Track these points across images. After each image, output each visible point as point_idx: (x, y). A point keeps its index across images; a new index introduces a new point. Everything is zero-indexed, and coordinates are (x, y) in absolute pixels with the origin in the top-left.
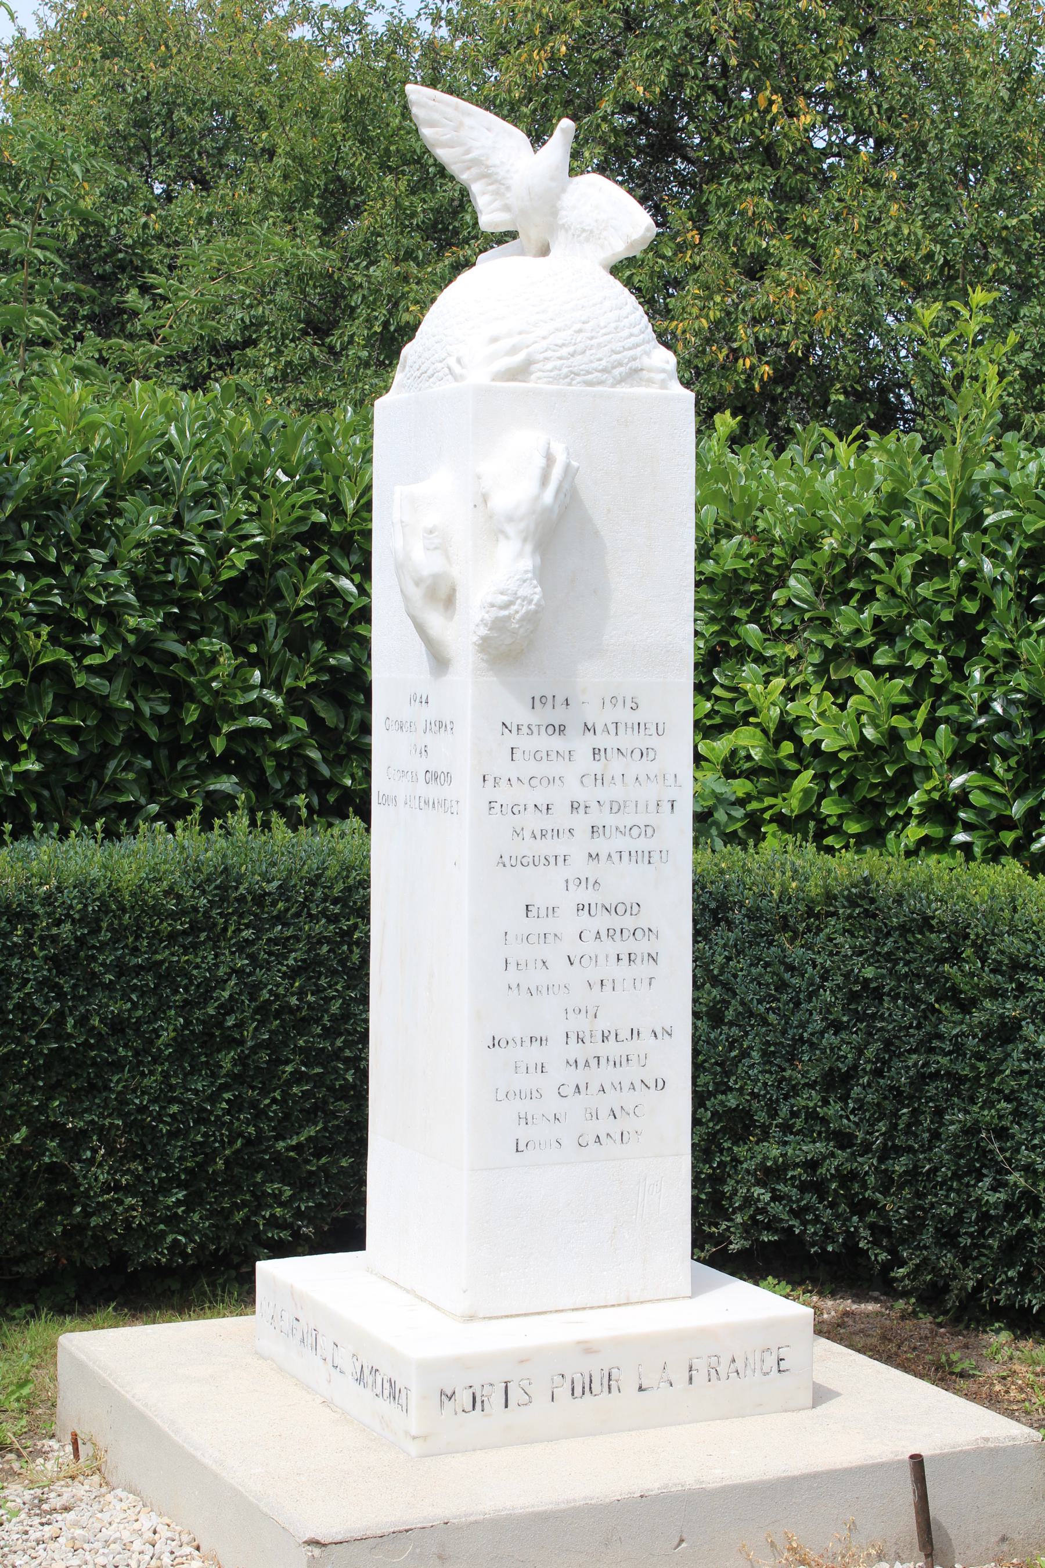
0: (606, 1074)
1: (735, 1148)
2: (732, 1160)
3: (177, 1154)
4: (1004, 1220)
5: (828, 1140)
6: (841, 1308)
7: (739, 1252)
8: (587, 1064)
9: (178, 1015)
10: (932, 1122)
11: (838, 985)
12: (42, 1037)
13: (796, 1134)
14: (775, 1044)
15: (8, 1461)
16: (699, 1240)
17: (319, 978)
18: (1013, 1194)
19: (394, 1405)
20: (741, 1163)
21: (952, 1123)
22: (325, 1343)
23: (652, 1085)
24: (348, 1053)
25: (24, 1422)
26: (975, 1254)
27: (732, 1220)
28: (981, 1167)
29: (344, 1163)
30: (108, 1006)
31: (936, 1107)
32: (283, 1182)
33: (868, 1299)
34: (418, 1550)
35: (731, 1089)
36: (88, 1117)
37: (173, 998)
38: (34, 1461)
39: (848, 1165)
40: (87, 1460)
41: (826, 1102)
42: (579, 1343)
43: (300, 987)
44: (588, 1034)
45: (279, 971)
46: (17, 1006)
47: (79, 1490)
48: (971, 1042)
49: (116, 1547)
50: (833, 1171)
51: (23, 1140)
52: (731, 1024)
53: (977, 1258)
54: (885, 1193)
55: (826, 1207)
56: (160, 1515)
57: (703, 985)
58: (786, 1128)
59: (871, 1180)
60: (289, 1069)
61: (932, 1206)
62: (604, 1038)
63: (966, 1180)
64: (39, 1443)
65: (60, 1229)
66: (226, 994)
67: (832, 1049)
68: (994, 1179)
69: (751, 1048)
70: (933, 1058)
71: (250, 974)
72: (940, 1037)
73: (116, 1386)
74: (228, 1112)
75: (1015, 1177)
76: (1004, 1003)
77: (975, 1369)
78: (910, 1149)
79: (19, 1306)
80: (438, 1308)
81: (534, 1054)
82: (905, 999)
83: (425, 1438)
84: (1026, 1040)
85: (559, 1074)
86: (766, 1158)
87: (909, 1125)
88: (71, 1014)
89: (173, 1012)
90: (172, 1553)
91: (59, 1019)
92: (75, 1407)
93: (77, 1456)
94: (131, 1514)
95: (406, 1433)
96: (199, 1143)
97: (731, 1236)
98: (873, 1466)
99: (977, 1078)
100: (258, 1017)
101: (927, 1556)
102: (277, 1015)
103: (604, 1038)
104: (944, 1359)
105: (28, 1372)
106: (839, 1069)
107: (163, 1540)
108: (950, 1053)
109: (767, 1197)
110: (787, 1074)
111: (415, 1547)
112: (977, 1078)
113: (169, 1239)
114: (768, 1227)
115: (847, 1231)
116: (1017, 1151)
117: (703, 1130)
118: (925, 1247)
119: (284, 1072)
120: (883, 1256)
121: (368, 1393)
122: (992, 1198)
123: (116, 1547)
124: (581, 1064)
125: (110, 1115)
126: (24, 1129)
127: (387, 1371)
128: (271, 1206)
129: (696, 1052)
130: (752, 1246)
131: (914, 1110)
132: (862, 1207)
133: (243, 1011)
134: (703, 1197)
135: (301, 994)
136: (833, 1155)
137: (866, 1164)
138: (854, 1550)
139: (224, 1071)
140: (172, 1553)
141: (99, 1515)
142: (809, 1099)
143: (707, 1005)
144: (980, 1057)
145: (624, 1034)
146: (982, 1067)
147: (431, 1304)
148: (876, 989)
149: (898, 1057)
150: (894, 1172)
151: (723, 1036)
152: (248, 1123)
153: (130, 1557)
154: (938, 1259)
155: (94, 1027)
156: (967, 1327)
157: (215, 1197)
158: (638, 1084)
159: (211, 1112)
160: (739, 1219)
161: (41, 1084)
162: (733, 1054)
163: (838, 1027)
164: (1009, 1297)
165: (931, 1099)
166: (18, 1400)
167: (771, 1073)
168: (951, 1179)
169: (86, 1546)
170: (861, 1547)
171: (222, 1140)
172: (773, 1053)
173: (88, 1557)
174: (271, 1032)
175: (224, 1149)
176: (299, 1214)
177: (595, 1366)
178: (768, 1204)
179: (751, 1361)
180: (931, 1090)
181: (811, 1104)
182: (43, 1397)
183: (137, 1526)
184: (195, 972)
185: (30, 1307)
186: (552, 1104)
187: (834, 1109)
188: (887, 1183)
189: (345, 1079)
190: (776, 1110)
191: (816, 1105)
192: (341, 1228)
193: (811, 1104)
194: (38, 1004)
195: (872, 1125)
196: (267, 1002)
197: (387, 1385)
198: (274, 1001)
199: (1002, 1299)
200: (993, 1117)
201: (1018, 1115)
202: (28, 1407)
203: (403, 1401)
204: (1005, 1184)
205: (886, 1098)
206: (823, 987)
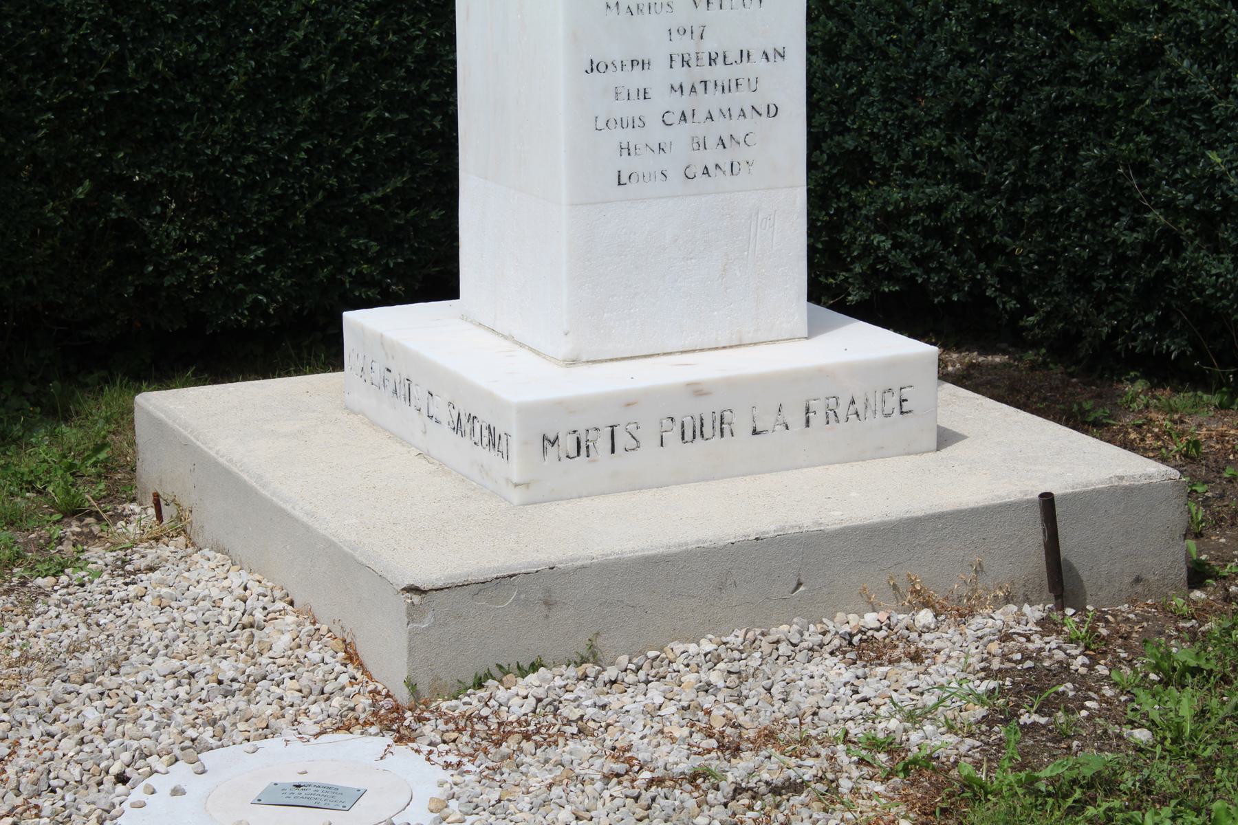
0: (713, 101)
1: (854, 194)
2: (850, 206)
3: (254, 209)
4: (1141, 262)
5: (953, 181)
6: (967, 360)
7: (858, 303)
8: (693, 89)
9: (248, 58)
10: (1065, 159)
11: (964, 14)
12: (101, 82)
13: (921, 175)
14: (896, 79)
15: (87, 525)
16: (816, 293)
17: (401, 16)
18: (1153, 234)
19: (493, 453)
20: (860, 209)
21: (1087, 159)
22: (418, 392)
23: (764, 111)
24: (434, 98)
25: (102, 486)
26: (1110, 299)
27: (849, 270)
28: (1118, 206)
29: (434, 216)
30: (172, 49)
31: (1070, 143)
32: (368, 237)
33: (994, 352)
34: (523, 596)
35: (848, 130)
36: (156, 170)
37: (242, 39)
38: (115, 524)
39: (974, 208)
40: (173, 523)
41: (950, 141)
42: (689, 385)
43: (380, 25)
44: (694, 57)
45: (357, 8)
46: (73, 49)
47: (164, 551)
48: (1109, 70)
49: (207, 604)
50: (958, 215)
51: (87, 195)
52: (848, 59)
53: (1111, 303)
54: (1014, 236)
55: (950, 254)
56: (251, 572)
57: (818, 17)
58: (908, 170)
59: (1000, 223)
60: (371, 115)
61: (1065, 249)
62: (712, 61)
63: (1102, 220)
64: (120, 508)
65: (131, 290)
66: (300, 34)
67: (958, 83)
68: (1132, 218)
69: (870, 84)
70: (1067, 89)
71: (325, 12)
72: (1075, 66)
73: (198, 443)
74: (307, 162)
75: (1156, 216)
76: (1146, 25)
77: (1109, 417)
78: (1041, 189)
79: (92, 373)
80: (538, 353)
81: (636, 79)
82: (1037, 26)
83: (527, 485)
84: (1169, 65)
85: (662, 100)
86: (886, 203)
87: (1040, 163)
88: (132, 57)
89: (243, 54)
90: (265, 609)
91: (119, 62)
92: (155, 467)
93: (159, 516)
94: (220, 572)
95: (508, 480)
96: (278, 196)
97: (842, 278)
98: (1000, 506)
99: (1115, 109)
100: (336, 59)
101: (1057, 597)
102: (357, 56)
103: (712, 61)
104: (1076, 407)
105: (105, 437)
106: (965, 105)
107: (254, 595)
108: (1086, 83)
109: (888, 245)
110: (909, 112)
111: (519, 593)
112: (1115, 109)
113: (249, 299)
114: (890, 277)
115: (974, 279)
116: (1158, 186)
117: (819, 174)
118: (1057, 293)
119: (366, 119)
120: (1012, 304)
121: (466, 442)
122: (1129, 238)
123: (207, 604)
124: (687, 89)
125: (180, 167)
126: (87, 183)
127: (485, 418)
128: (357, 263)
129: (810, 90)
130: (871, 297)
131: (1046, 147)
132: (988, 252)
133: (320, 53)
134: (820, 246)
135: (382, 34)
136: (958, 197)
137: (994, 207)
138: (980, 591)
139: (301, 118)
140: (265, 609)
141: (186, 574)
142: (933, 138)
143: (822, 39)
144: (1118, 87)
145: (733, 56)
146: (1120, 97)
147: (531, 349)
148: (1006, 15)
149: (1030, 89)
150: (1024, 214)
151: (840, 72)
152: (329, 174)
153: (221, 614)
154: (1070, 305)
155: (157, 72)
156: (1101, 377)
157: (297, 254)
158: (748, 111)
159: (289, 163)
160: (858, 269)
161: (103, 134)
162: (851, 91)
163: (964, 59)
164: (1145, 343)
165: (1065, 134)
166: (94, 465)
167: (892, 111)
168: (1085, 220)
169: (173, 604)
170: (987, 590)
171: (302, 193)
172: (894, 89)
173: (176, 614)
174: (350, 75)
175: (305, 202)
176: (387, 272)
177: (705, 408)
178: (889, 252)
179: (871, 401)
180: (1065, 123)
181: (935, 144)
182: (122, 461)
183: (226, 583)
184: (265, 10)
185: (104, 373)
186: (656, 133)
187: (960, 147)
188: (1016, 226)
189: (433, 126)
190: (896, 150)
191: (940, 145)
192: (430, 273)
193: (935, 144)
194: (95, 46)
195: (1001, 165)
196: (345, 41)
197: (486, 433)
198: (353, 42)
199: (1138, 346)
200: (1131, 151)
201: (1159, 148)
202: (106, 470)
203: (503, 447)
204: (1143, 223)
205: (1015, 134)
206: (948, 15)
